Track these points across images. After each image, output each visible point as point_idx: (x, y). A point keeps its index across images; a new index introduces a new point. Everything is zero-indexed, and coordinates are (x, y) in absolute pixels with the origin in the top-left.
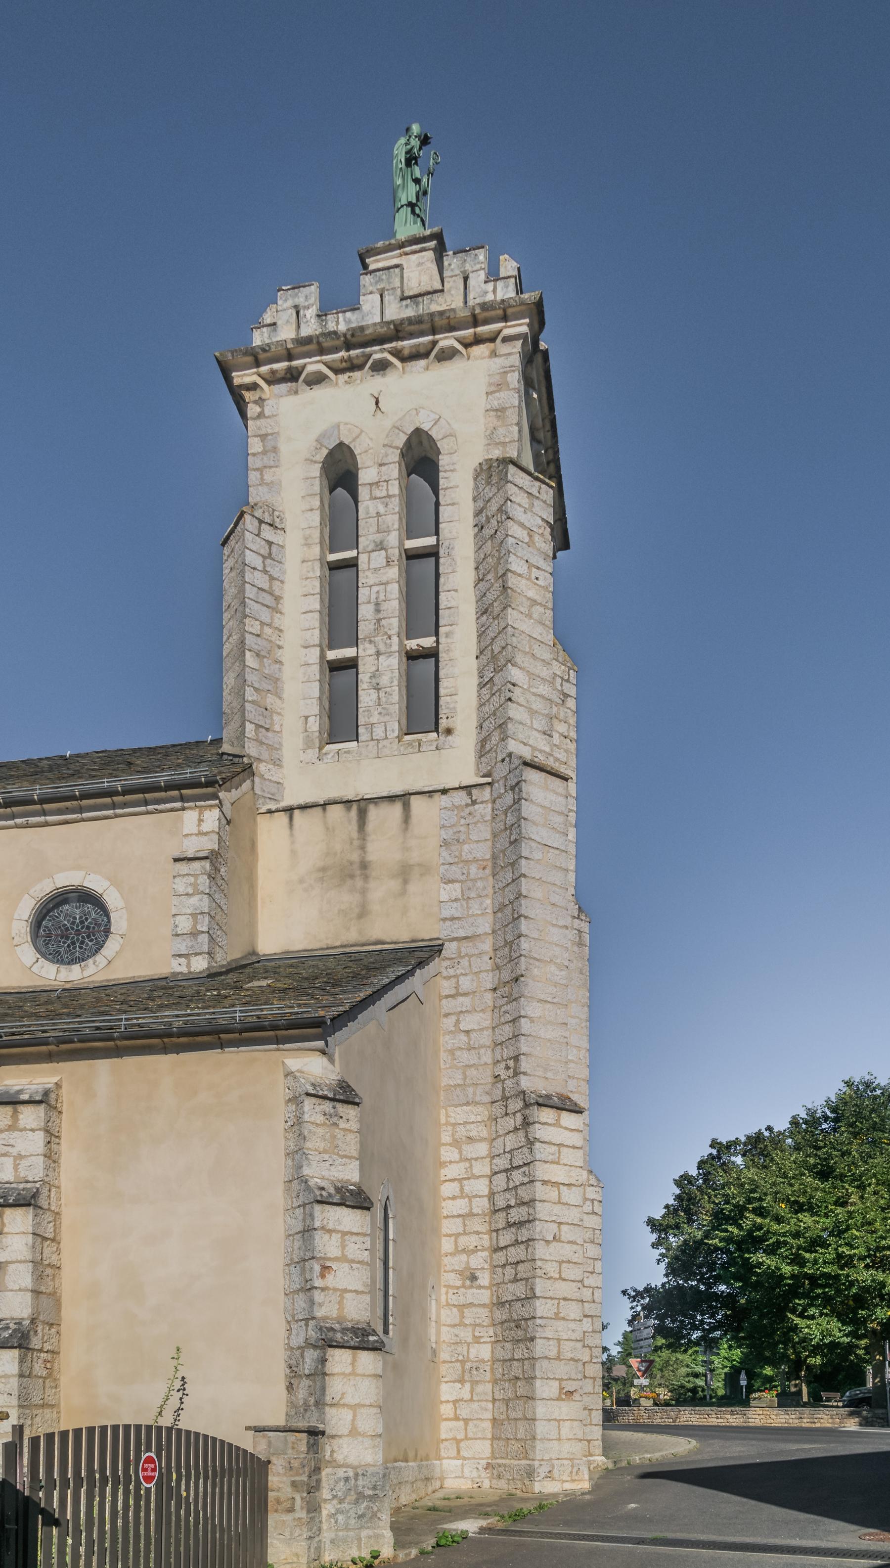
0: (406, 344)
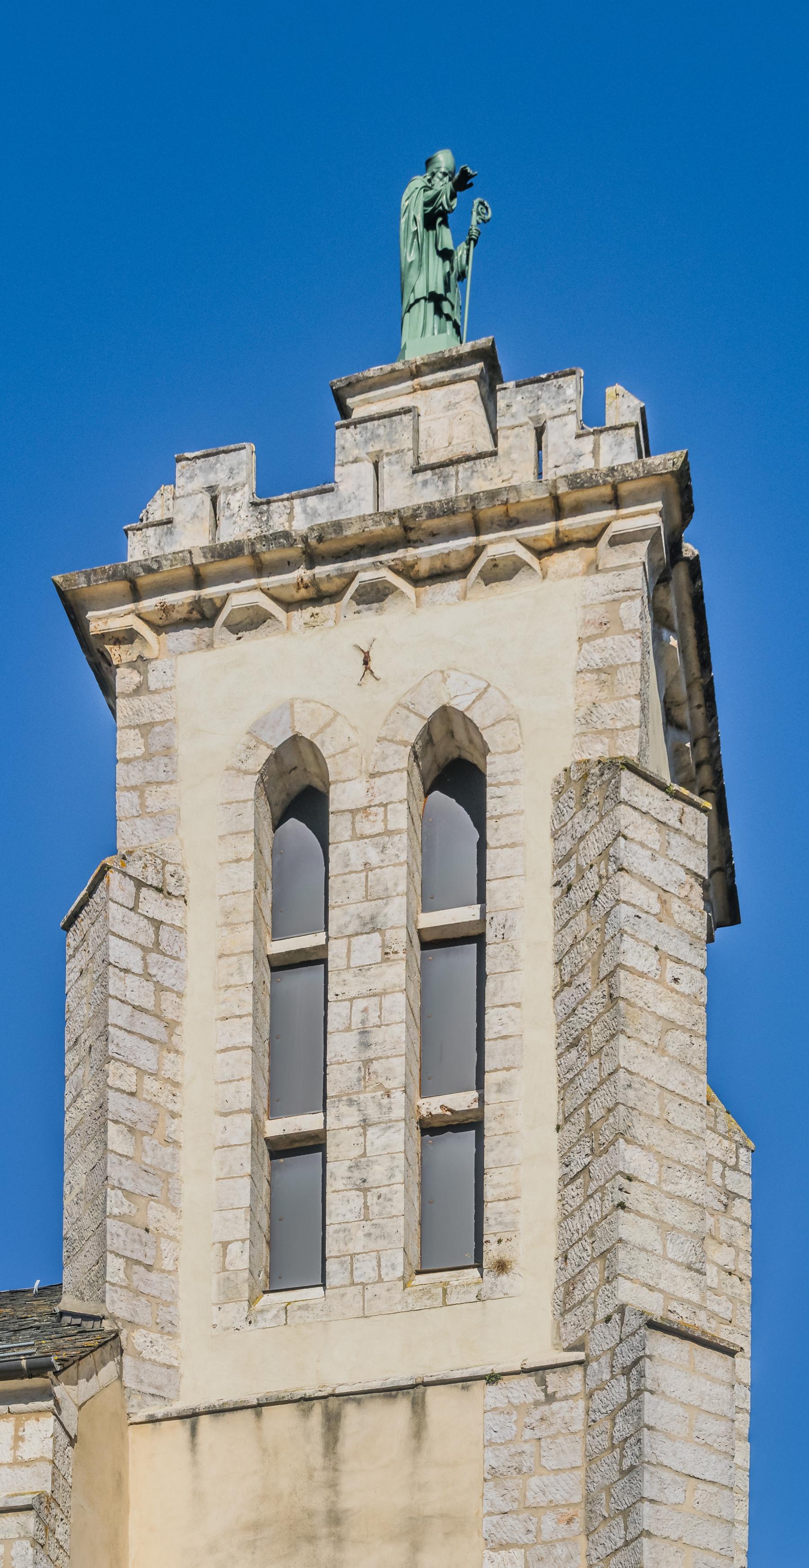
0: (424, 555)
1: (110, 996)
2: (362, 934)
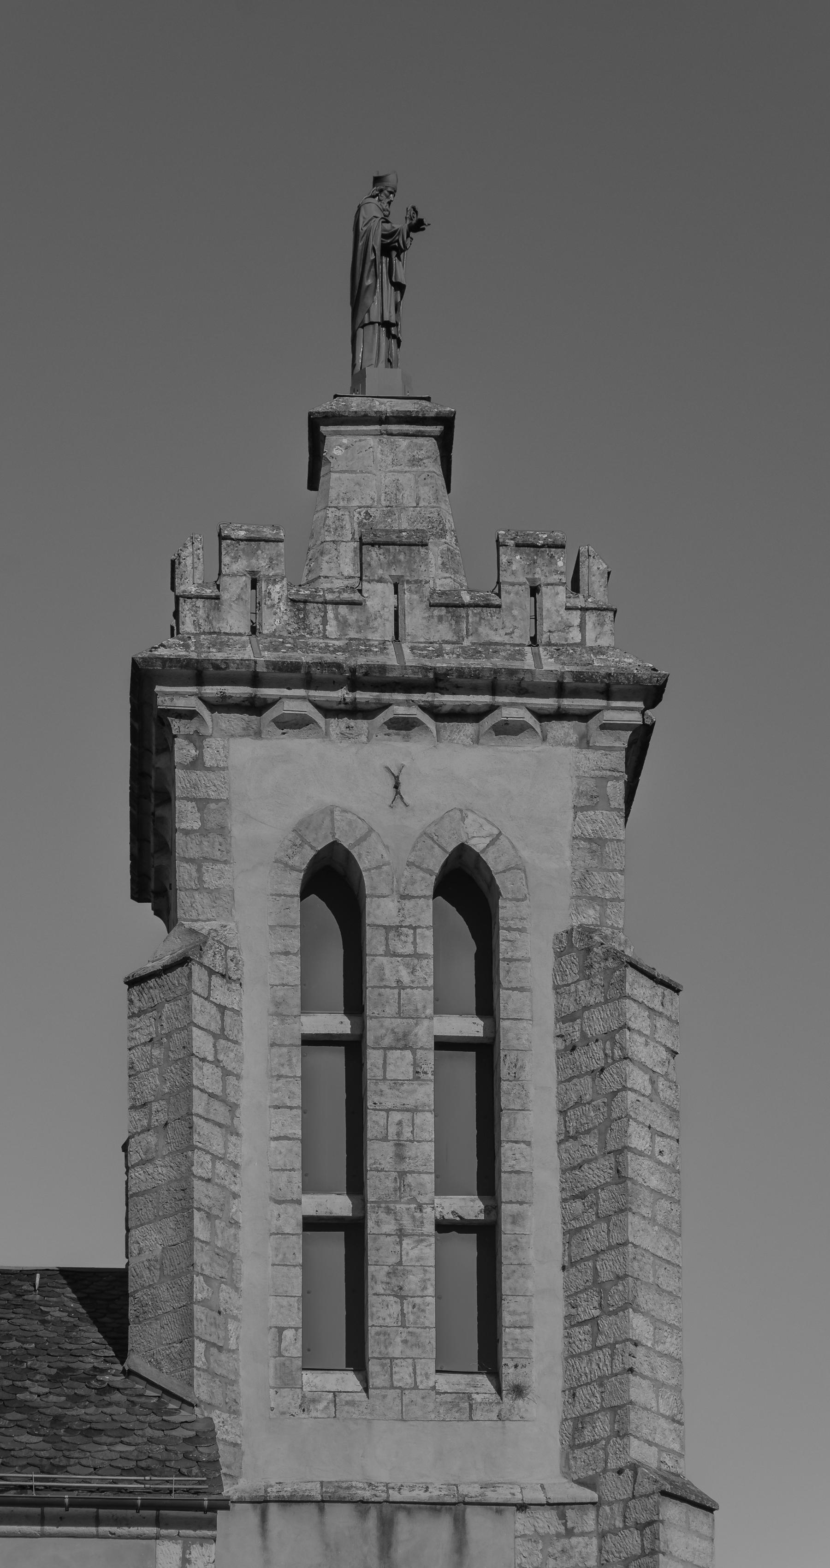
0: (449, 700)
1: (193, 1086)
2: (396, 1049)
